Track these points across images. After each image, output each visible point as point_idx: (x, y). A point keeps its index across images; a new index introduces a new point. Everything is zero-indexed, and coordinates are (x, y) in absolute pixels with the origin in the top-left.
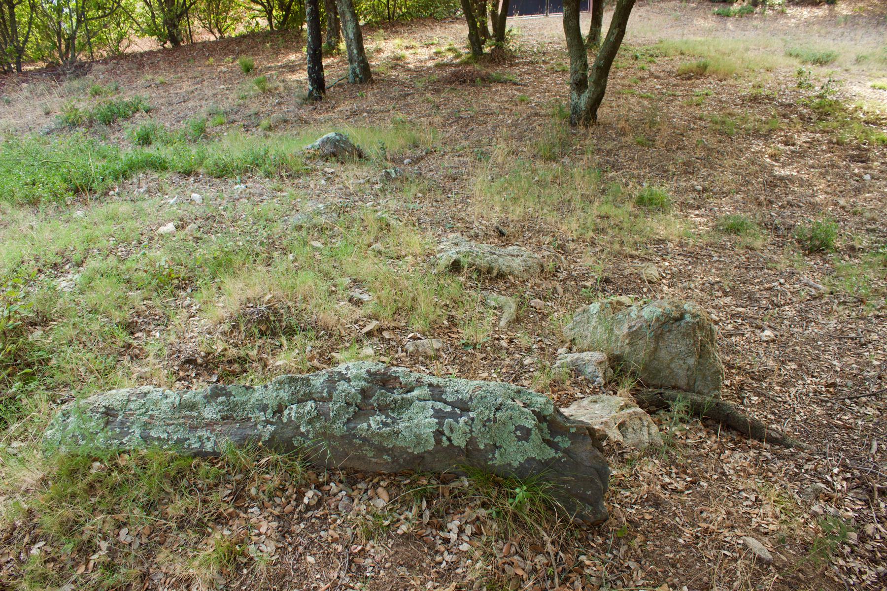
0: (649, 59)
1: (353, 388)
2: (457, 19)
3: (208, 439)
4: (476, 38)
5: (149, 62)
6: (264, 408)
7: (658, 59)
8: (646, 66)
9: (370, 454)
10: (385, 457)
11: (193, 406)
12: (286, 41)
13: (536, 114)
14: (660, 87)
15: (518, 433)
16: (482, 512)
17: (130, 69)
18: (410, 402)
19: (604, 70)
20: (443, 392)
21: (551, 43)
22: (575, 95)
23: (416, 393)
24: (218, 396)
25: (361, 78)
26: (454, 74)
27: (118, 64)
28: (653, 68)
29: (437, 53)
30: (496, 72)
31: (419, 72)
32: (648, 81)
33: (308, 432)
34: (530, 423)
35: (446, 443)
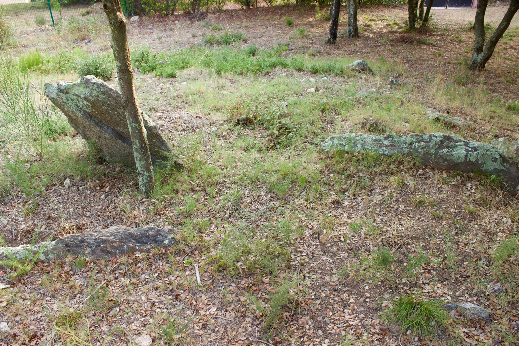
0: (510, 38)
1: (438, 139)
2: (396, 6)
3: (386, 151)
4: (413, 17)
5: (236, 15)
6: (406, 143)
7: (515, 38)
8: (508, 42)
9: (441, 161)
10: (446, 163)
11: (380, 140)
12: (305, 11)
13: (449, 63)
14: (516, 54)
15: (493, 159)
16: (478, 183)
17: (227, 18)
18: (457, 146)
19: (494, 43)
20: (468, 144)
21: (451, 24)
22: (475, 55)
23: (459, 143)
24: (389, 138)
25: (353, 35)
26: (401, 38)
27: (220, 15)
28: (512, 43)
29: (388, 25)
30: (424, 38)
31: (380, 35)
32: (509, 50)
33: (421, 151)
34: (498, 157)
35: (468, 160)
